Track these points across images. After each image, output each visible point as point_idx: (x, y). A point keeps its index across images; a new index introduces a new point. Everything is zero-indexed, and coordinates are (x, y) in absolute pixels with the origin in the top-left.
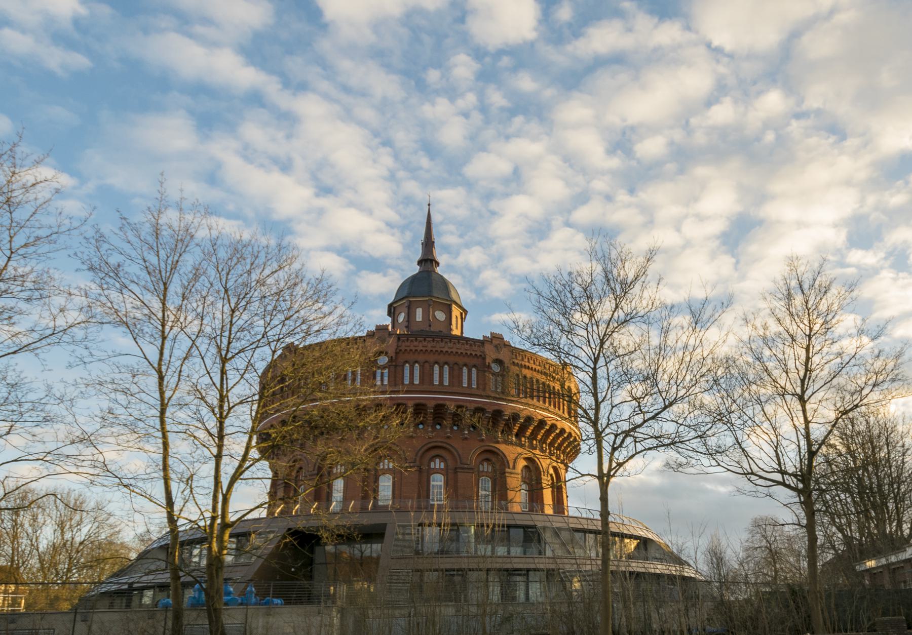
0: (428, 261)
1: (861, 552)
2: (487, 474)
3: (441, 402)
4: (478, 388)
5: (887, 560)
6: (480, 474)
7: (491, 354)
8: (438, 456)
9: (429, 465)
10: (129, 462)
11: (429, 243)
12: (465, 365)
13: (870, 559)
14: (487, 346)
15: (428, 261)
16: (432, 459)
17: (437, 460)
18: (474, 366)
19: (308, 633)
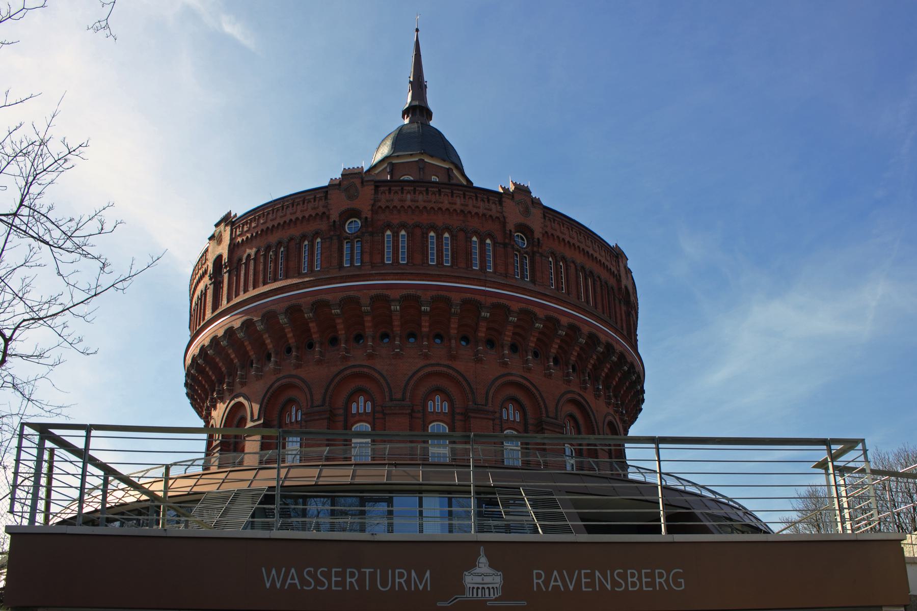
0: (419, 110)
1: (335, 235)
2: (512, 425)
3: (412, 292)
4: (495, 272)
5: (42, 499)
6: (502, 425)
7: (513, 215)
8: (439, 390)
9: (425, 406)
10: (112, 392)
11: (418, 85)
12: (433, 228)
13: (431, 574)
14: (507, 202)
15: (419, 110)
16: (429, 395)
17: (438, 398)
18: (448, 229)
19: (0, 601)
